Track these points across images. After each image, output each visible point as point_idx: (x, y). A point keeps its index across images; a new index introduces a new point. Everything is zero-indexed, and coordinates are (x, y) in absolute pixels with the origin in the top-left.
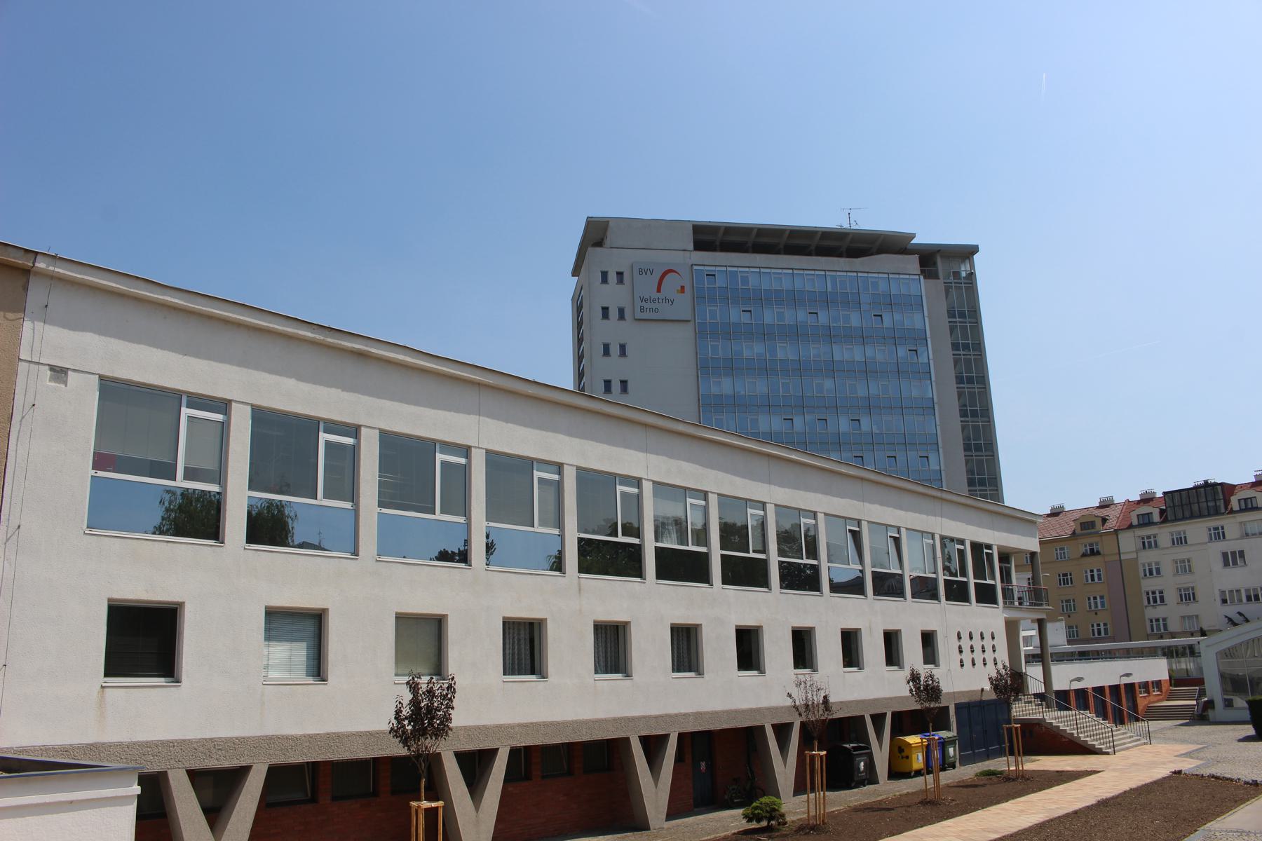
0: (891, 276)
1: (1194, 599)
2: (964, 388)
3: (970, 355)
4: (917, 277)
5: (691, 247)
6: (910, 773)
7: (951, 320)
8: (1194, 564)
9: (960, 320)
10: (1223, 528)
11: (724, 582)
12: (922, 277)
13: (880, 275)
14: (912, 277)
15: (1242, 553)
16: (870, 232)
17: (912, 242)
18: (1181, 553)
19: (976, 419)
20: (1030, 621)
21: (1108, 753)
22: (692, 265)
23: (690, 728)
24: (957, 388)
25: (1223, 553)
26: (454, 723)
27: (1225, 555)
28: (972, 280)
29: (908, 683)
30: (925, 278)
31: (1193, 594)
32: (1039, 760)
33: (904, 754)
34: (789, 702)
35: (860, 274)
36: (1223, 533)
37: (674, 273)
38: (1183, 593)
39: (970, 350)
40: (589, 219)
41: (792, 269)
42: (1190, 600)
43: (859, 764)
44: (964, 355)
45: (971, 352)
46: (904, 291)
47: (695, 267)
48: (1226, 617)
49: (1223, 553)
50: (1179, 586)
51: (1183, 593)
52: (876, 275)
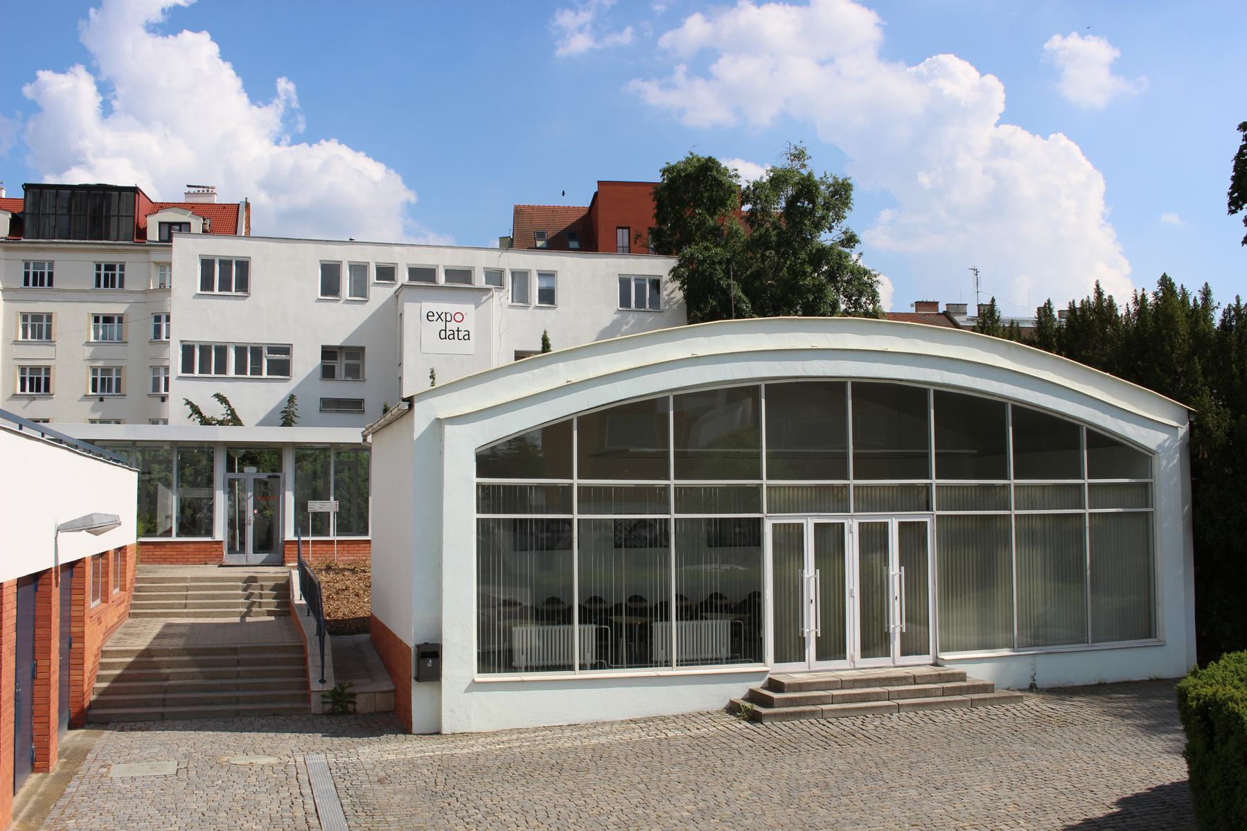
10: (122, 268)
36: (122, 277)
48: (188, 403)
51: (31, 271)
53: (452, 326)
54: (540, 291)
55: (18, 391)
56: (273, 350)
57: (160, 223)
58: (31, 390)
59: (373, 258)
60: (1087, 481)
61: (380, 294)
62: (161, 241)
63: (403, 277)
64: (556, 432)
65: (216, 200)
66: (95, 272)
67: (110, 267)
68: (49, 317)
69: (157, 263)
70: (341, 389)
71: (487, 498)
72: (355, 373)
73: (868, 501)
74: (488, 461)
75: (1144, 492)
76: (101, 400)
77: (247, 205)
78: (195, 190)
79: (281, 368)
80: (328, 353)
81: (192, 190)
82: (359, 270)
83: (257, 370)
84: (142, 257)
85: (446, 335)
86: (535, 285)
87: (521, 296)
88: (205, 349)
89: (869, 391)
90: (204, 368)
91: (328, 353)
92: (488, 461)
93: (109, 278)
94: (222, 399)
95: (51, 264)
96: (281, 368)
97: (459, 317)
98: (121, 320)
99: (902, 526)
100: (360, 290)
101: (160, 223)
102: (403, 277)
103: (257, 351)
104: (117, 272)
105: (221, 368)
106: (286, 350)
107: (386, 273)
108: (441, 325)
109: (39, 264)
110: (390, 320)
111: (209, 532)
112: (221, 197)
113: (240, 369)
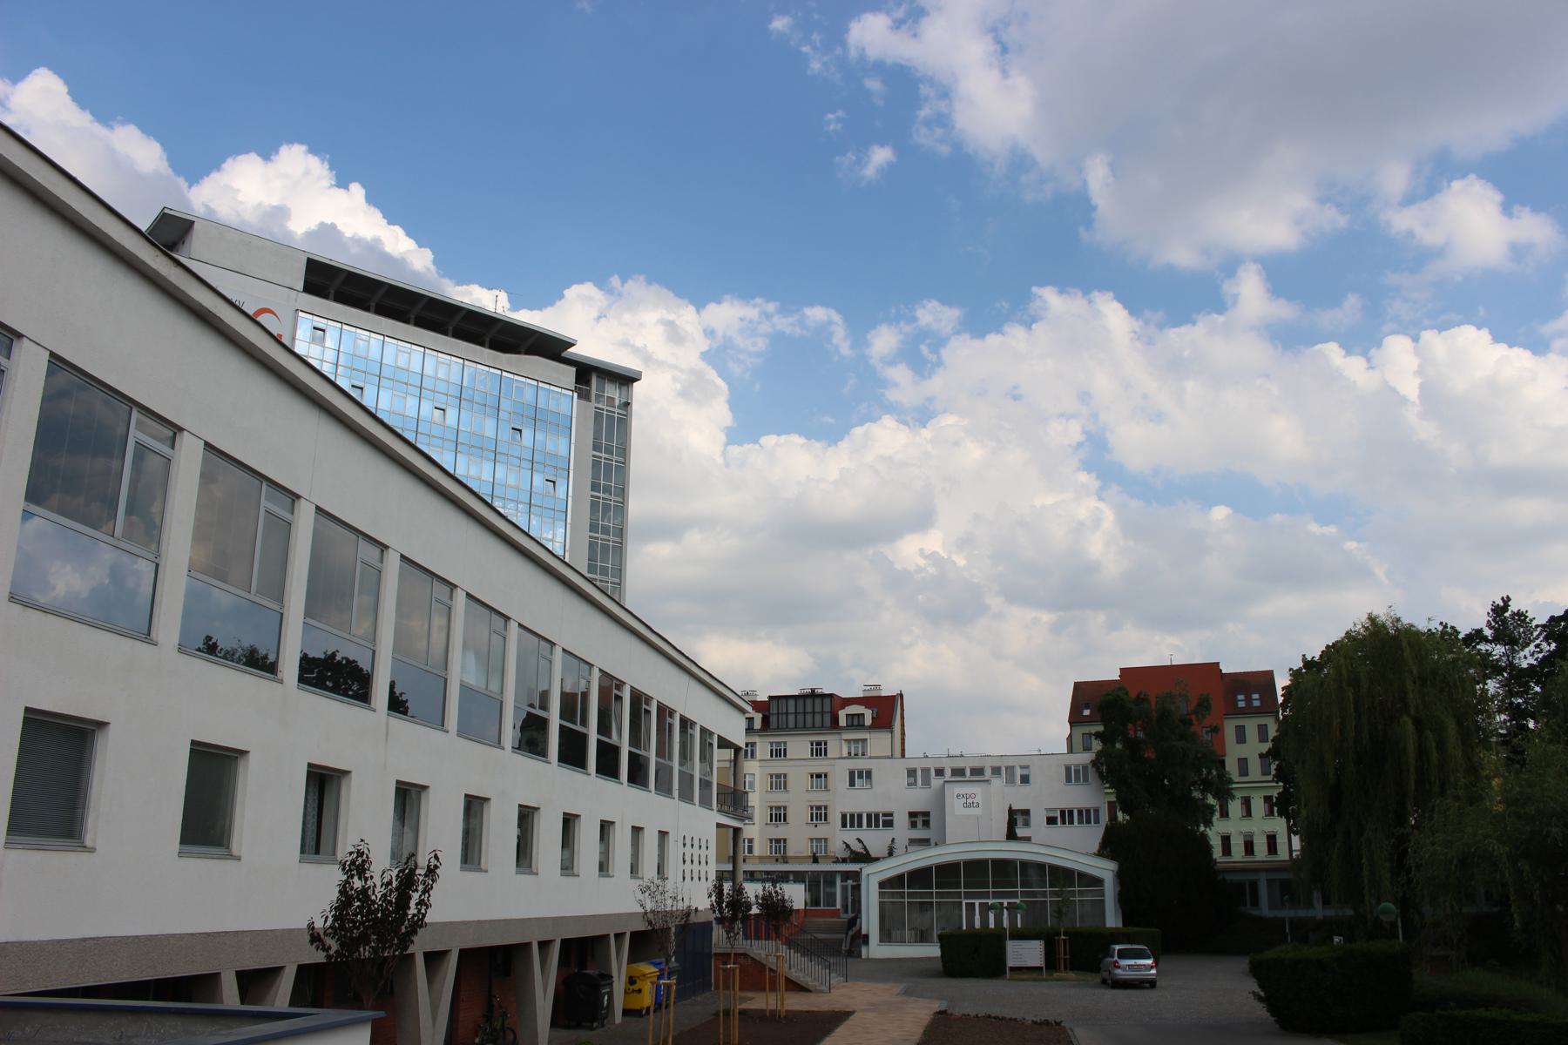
0: (541, 384)
1: (785, 820)
2: (598, 538)
3: (611, 500)
4: (570, 393)
5: (300, 285)
6: (641, 1011)
7: (595, 453)
8: (905, 780)
9: (607, 456)
10: (826, 744)
11: (560, 760)
12: (576, 395)
13: (529, 381)
14: (564, 391)
15: (869, 774)
16: (561, 338)
17: (569, 350)
18: (779, 767)
19: (604, 578)
20: (1033, 840)
21: (822, 992)
22: (297, 310)
23: (471, 943)
24: (590, 537)
25: (1028, 782)
26: (427, 920)
27: (852, 774)
28: (627, 411)
29: (710, 896)
30: (579, 397)
31: (785, 814)
32: (751, 999)
33: (636, 987)
34: (641, 910)
35: (504, 374)
36: (826, 749)
37: (271, 315)
38: (774, 813)
39: (611, 495)
40: (166, 211)
41: (463, 359)
42: (780, 821)
43: (604, 998)
44: (603, 499)
45: (613, 498)
46: (552, 406)
47: (301, 314)
48: (845, 843)
49: (1028, 782)
50: (772, 804)
51: (774, 813)
52: (523, 379)
53: (970, 801)
54: (1021, 776)
55: (769, 822)
56: (884, 815)
57: (847, 715)
58: (776, 821)
59: (932, 765)
60: (1077, 889)
61: (936, 782)
62: (847, 726)
63: (948, 773)
64: (900, 877)
65: (884, 694)
66: (810, 747)
67: (819, 744)
68: (785, 776)
69: (845, 740)
70: (919, 833)
71: (881, 895)
72: (926, 824)
73: (968, 895)
74: (882, 885)
75: (1102, 893)
76: (816, 826)
77: (901, 695)
78: (869, 688)
79: (889, 824)
80: (912, 815)
81: (867, 688)
82: (926, 771)
83: (877, 825)
84: (837, 737)
85: (967, 805)
86: (1019, 772)
87: (1010, 780)
88: (852, 816)
89: (996, 862)
90: (852, 825)
91: (912, 815)
92: (882, 885)
93: (819, 750)
94: (860, 841)
95: (785, 743)
96: (889, 824)
97: (973, 796)
98: (826, 776)
99: (980, 904)
100: (927, 782)
101: (847, 715)
102: (948, 773)
103: (877, 816)
104: (823, 747)
105: (860, 825)
106: (891, 815)
107: (940, 772)
108: (964, 800)
109: (778, 743)
110: (941, 796)
111: (835, 906)
112: (886, 692)
113: (869, 825)
